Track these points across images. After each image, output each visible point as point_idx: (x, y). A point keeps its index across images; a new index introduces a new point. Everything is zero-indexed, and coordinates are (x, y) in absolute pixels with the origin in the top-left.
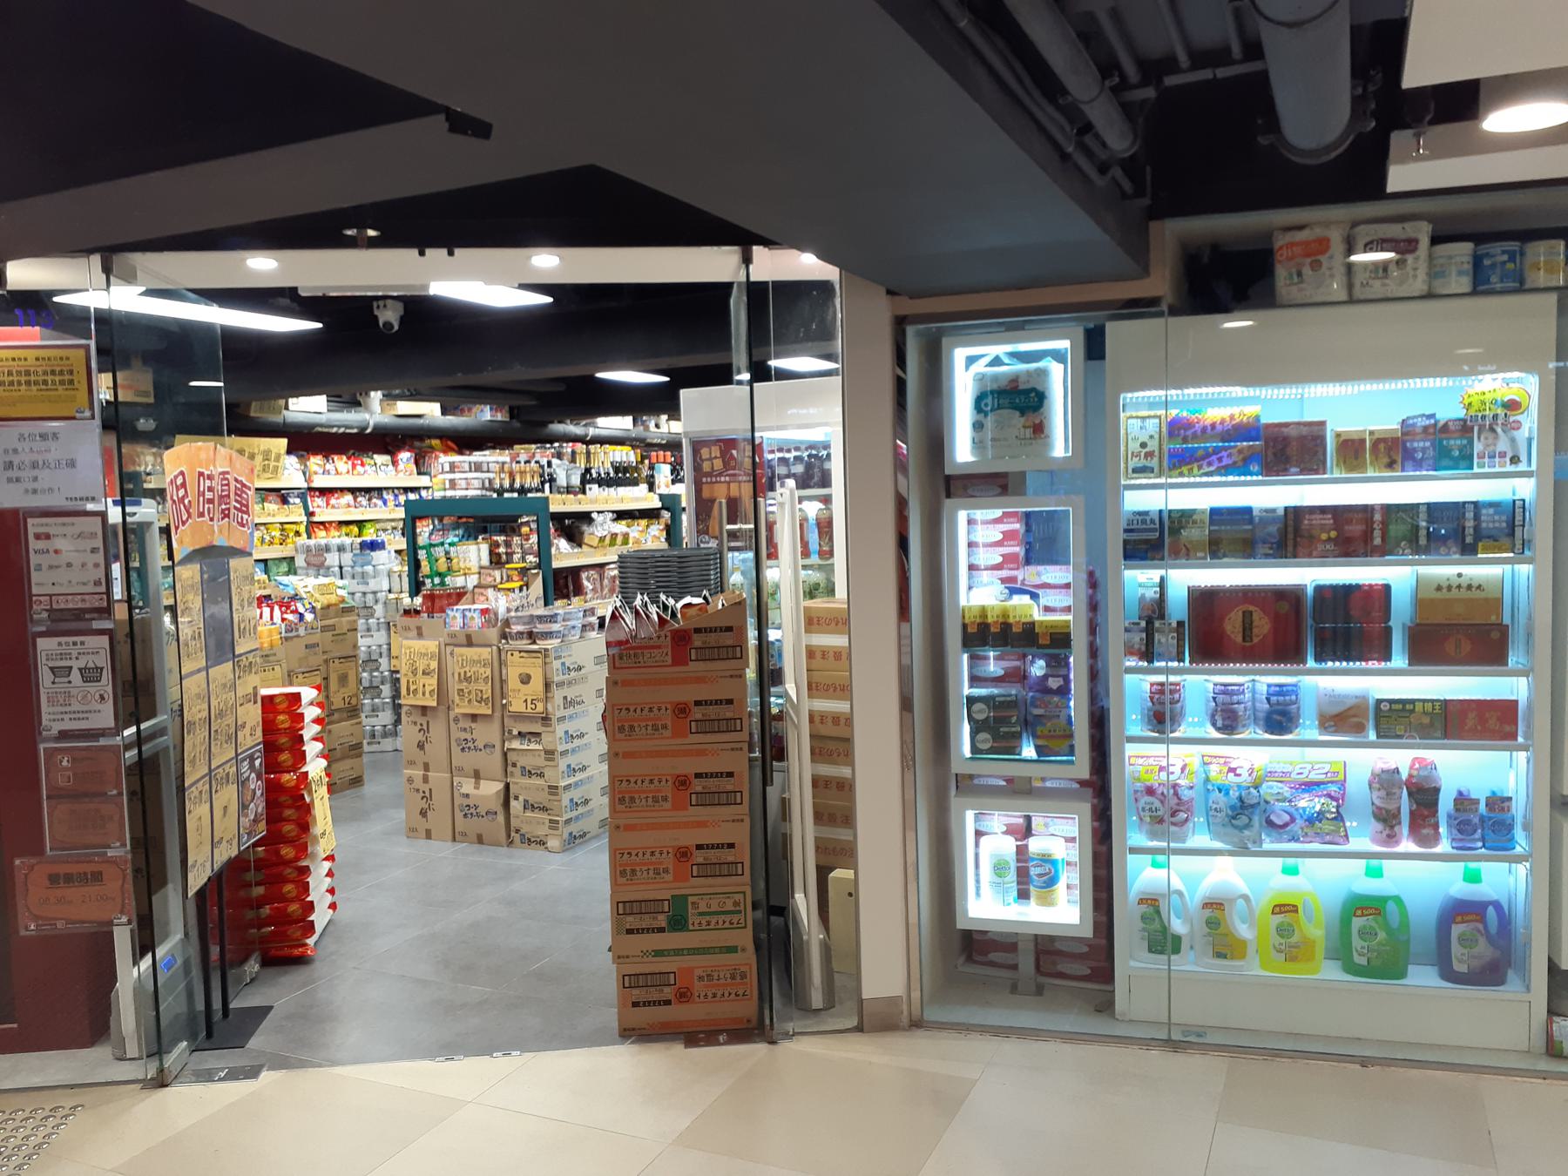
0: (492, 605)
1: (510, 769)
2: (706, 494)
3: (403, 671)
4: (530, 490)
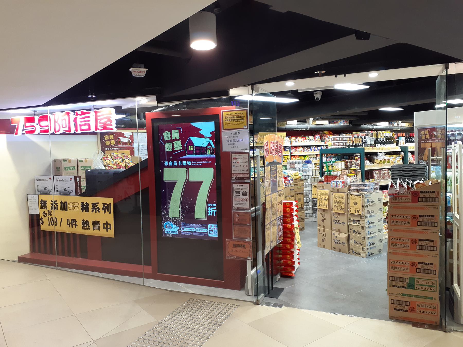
0: (345, 180)
1: (350, 230)
2: (422, 146)
3: (318, 199)
4: (358, 146)
